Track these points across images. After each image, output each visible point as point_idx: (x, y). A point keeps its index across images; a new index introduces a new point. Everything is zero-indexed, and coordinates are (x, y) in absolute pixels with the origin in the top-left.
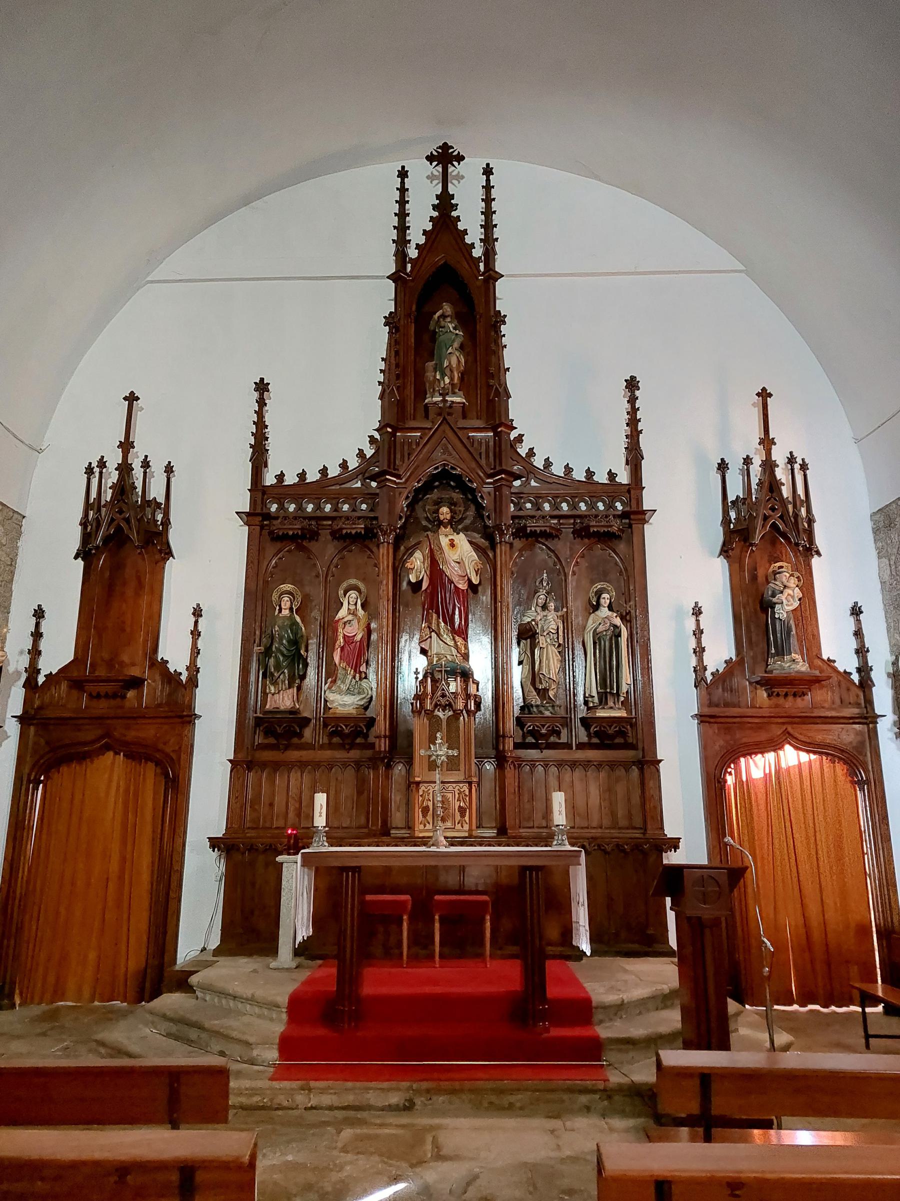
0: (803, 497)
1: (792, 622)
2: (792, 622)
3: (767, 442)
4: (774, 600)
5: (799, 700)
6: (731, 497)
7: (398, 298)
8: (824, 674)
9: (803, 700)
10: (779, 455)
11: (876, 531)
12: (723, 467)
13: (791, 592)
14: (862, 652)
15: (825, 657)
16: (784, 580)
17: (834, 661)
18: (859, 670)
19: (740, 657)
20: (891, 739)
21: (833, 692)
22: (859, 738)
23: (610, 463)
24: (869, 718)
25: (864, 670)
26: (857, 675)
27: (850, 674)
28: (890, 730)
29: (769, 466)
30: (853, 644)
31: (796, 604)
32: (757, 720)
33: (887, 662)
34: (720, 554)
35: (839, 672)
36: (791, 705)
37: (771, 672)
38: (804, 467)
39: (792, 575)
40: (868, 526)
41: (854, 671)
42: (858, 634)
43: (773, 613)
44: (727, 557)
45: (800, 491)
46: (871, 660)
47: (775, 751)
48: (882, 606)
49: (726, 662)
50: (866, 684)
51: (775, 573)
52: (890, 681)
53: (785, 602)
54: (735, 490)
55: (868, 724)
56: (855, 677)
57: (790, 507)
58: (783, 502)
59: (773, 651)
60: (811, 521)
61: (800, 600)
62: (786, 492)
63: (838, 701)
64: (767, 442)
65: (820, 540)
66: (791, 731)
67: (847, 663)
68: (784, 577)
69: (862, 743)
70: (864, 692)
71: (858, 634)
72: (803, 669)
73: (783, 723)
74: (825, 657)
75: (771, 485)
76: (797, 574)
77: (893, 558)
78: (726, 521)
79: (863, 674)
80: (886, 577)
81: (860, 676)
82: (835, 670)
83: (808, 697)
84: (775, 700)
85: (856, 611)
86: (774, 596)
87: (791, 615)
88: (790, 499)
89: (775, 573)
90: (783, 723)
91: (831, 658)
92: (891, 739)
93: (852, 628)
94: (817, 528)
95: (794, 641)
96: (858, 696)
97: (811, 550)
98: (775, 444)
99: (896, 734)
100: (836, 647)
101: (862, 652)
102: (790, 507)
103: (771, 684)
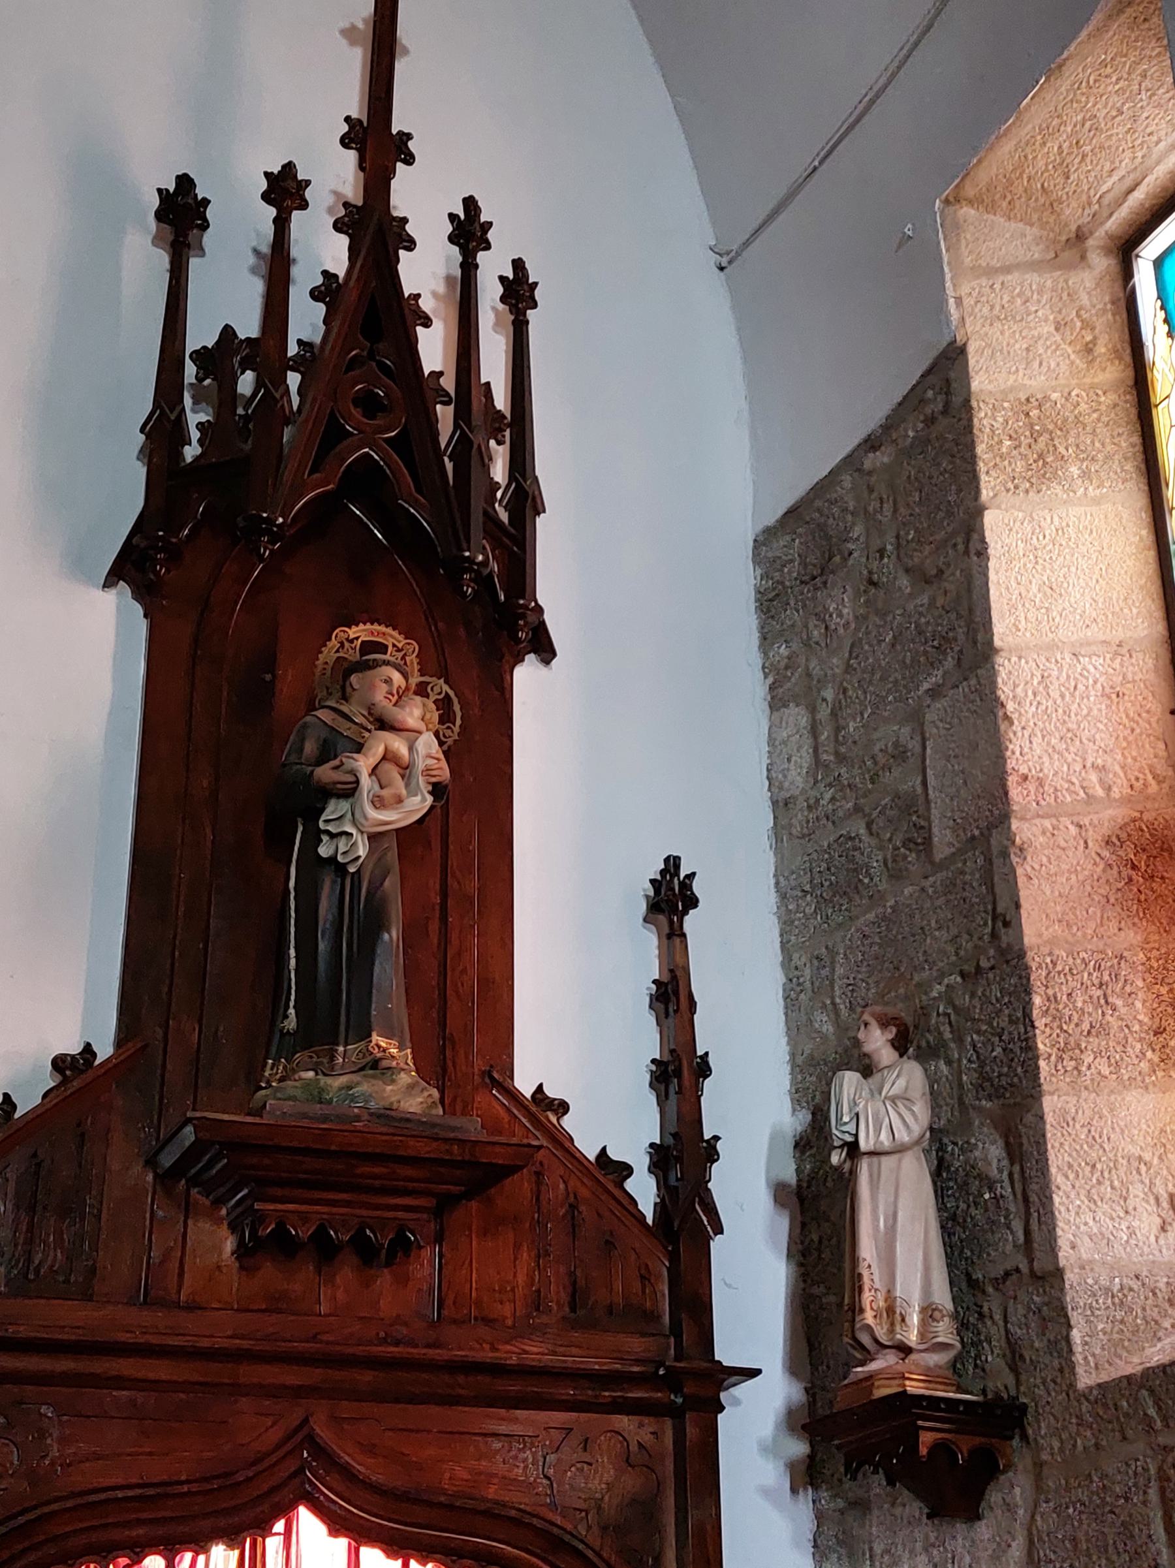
0: (501, 400)
1: (391, 884)
2: (391, 884)
3: (378, 143)
4: (325, 773)
5: (384, 1280)
6: (201, 334)
7: (52, 1095)
8: (504, 1156)
9: (403, 1280)
10: (421, 199)
11: (769, 603)
12: (182, 214)
13: (399, 745)
14: (679, 1074)
15: (525, 1085)
16: (380, 696)
17: (562, 1107)
18: (661, 1159)
19: (131, 1047)
20: (766, 1492)
21: (541, 1255)
22: (631, 1483)
23: (364, 1551)
24: (697, 1385)
25: (685, 1154)
26: (651, 1182)
27: (626, 1170)
28: (766, 1450)
29: (375, 231)
30: (648, 1043)
31: (419, 804)
32: (162, 1370)
33: (774, 1137)
34: (114, 577)
35: (575, 1157)
36: (335, 1300)
37: (259, 1111)
38: (519, 292)
39: (422, 690)
40: (742, 581)
41: (640, 1162)
42: (672, 998)
43: (314, 836)
44: (145, 593)
45: (494, 367)
46: (717, 1111)
47: (232, 1538)
48: (772, 898)
49: (60, 1063)
50: (688, 1218)
51: (345, 670)
52: (783, 1224)
53: (366, 781)
54: (225, 300)
55: (676, 1414)
56: (644, 1190)
57: (445, 414)
58: (418, 388)
59: (291, 1023)
60: (526, 500)
61: (437, 790)
62: (434, 349)
63: (557, 1294)
64: (378, 143)
65: (555, 589)
66: (323, 1432)
67: (614, 1122)
68: (386, 683)
69: (644, 1510)
70: (674, 1257)
71: (672, 998)
72: (414, 1104)
73: (299, 1393)
74: (525, 1085)
75: (372, 303)
76: (441, 687)
77: (829, 694)
78: (163, 431)
79: (676, 1173)
80: (797, 779)
81: (663, 1185)
82: (563, 1142)
83: (427, 1264)
84: (269, 1272)
85: (671, 898)
86: (327, 753)
87: (393, 856)
88: (448, 383)
89: (345, 670)
90: (299, 1393)
91: (550, 1092)
92: (766, 1492)
93: (648, 967)
94: (550, 537)
95: (388, 972)
96: (646, 1277)
97: (509, 627)
98: (409, 159)
99: (792, 1467)
100: (572, 1041)
101: (679, 1074)
102: (445, 414)
103: (252, 1171)
